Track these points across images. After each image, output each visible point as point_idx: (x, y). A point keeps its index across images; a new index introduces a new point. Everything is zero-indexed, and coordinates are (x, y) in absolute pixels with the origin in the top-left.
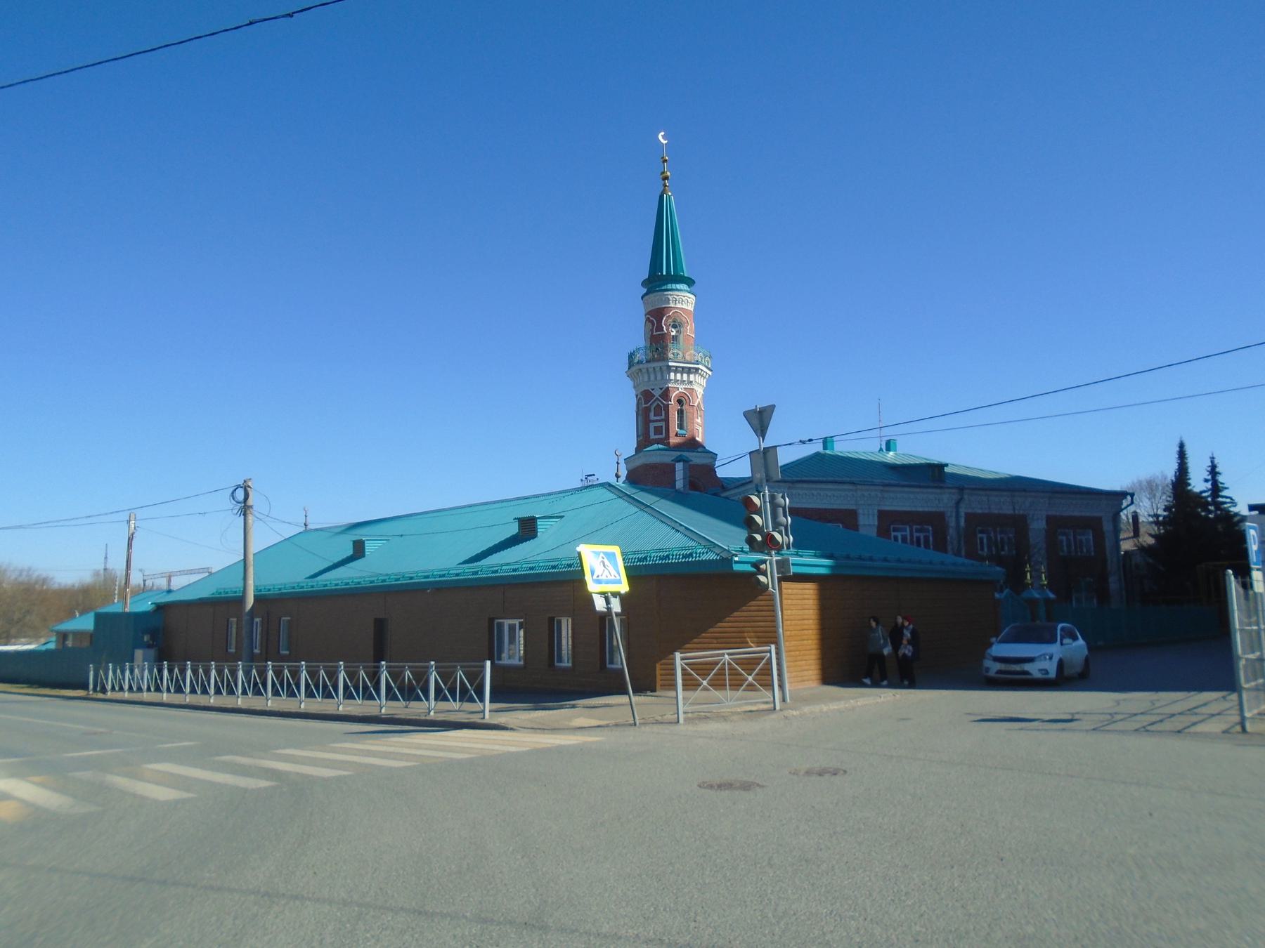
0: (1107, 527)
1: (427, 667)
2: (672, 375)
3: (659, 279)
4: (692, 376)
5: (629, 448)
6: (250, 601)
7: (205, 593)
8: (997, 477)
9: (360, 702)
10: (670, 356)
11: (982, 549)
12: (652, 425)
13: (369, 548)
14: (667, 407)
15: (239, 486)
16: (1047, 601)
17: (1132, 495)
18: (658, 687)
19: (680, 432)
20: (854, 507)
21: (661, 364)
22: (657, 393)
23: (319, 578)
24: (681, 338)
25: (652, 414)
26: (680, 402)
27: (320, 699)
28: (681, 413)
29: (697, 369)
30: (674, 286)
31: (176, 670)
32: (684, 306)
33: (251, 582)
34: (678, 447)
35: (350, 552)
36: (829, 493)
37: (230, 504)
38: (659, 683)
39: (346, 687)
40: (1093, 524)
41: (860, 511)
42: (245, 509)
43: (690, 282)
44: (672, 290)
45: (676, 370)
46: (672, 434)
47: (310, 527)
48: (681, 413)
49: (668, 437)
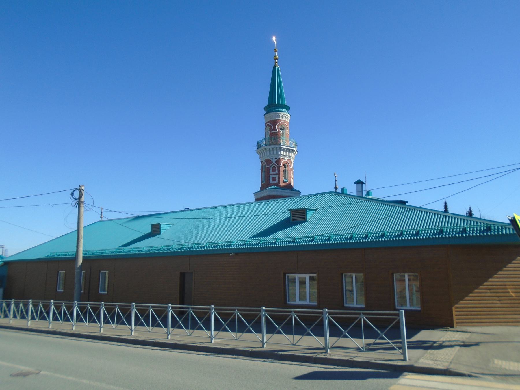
1: (10, 302)
2: (282, 152)
3: (274, 105)
4: (290, 154)
5: (258, 188)
6: (80, 261)
7: (42, 254)
9: (87, 324)
10: (281, 143)
12: (271, 177)
13: (163, 228)
14: (279, 168)
15: (76, 189)
18: (455, 324)
19: (285, 180)
21: (277, 146)
22: (274, 161)
23: (131, 246)
25: (271, 171)
26: (284, 166)
27: (61, 322)
28: (285, 171)
29: (293, 150)
30: (282, 110)
31: (21, 305)
32: (286, 120)
33: (81, 248)
34: (284, 188)
35: (149, 230)
37: (70, 200)
38: (455, 321)
39: (78, 315)
42: (79, 203)
43: (288, 108)
44: (281, 111)
45: (284, 150)
46: (281, 181)
47: (103, 219)
48: (285, 171)
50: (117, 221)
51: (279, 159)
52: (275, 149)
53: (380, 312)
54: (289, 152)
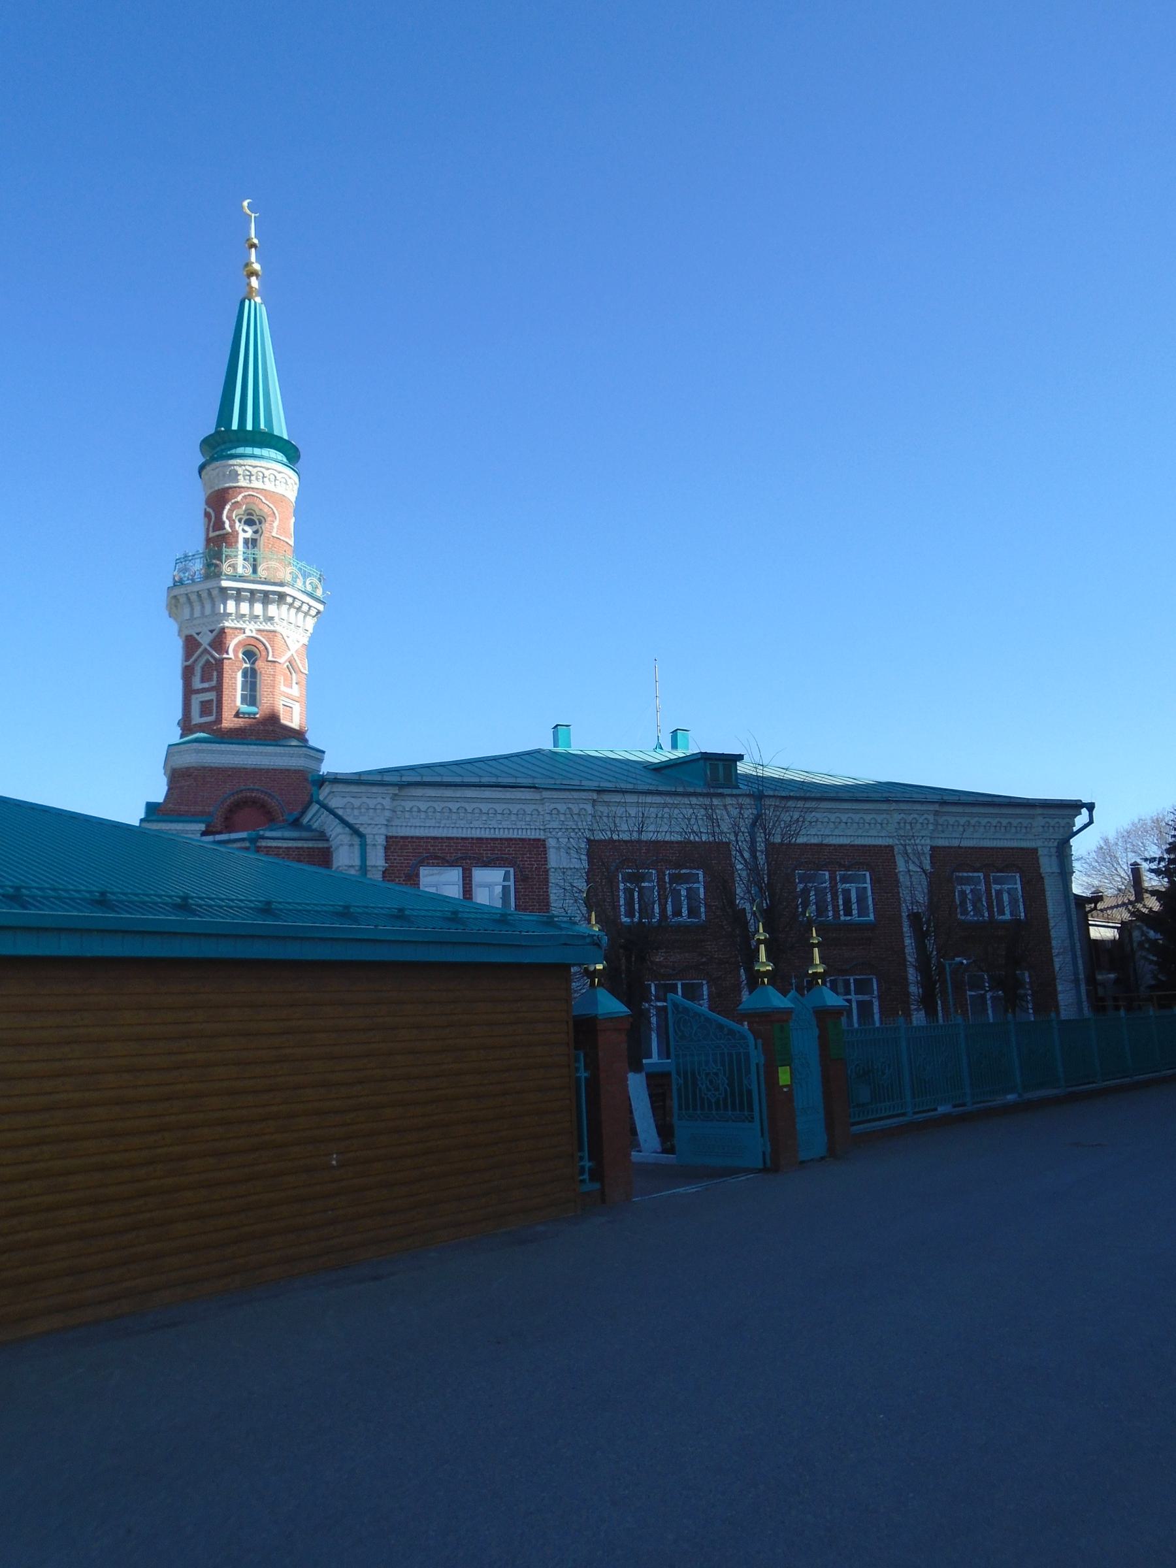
0: (1047, 865)
8: (850, 782)
11: (1002, 913)
16: (824, 1015)
17: (1091, 807)
20: (541, 835)
21: (210, 584)
22: (205, 640)
24: (262, 542)
26: (250, 655)
28: (251, 676)
30: (249, 450)
32: (269, 486)
36: (485, 807)
40: (1023, 863)
41: (551, 842)
45: (238, 596)
49: (219, 720)
50: (666, 771)
51: (222, 631)
52: (204, 595)
53: (762, 1078)
54: (252, 601)
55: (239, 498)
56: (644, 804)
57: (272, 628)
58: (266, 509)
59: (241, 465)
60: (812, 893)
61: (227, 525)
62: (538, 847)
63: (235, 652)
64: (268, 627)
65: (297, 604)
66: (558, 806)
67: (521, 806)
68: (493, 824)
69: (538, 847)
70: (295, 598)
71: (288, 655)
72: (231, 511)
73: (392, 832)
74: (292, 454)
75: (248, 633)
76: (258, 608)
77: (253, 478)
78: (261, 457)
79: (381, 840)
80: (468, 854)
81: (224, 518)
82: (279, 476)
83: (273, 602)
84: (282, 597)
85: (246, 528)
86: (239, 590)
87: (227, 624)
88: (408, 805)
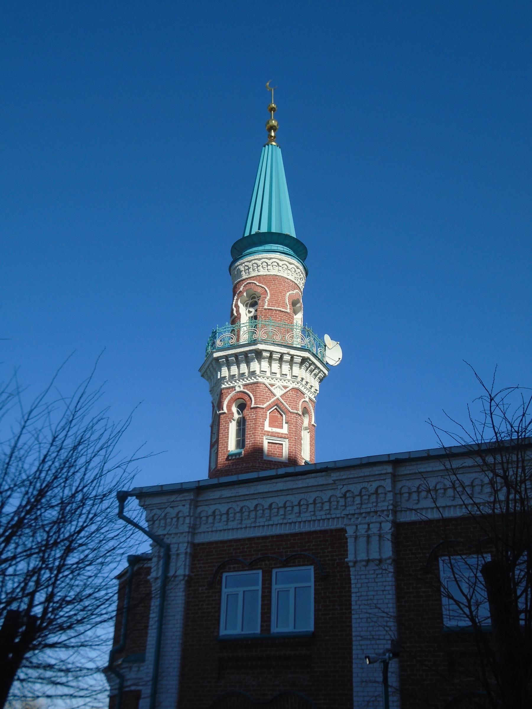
26: (242, 407)
32: (263, 272)
36: (280, 501)
41: (350, 531)
55: (241, 289)
56: (454, 471)
57: (255, 380)
58: (259, 290)
59: (241, 264)
60: (522, 616)
61: (235, 312)
62: (337, 538)
63: (229, 407)
64: (253, 380)
65: (276, 356)
66: (351, 487)
67: (302, 496)
68: (292, 518)
69: (337, 538)
70: (271, 352)
71: (275, 398)
72: (237, 299)
73: (200, 539)
74: (297, 248)
75: (238, 389)
76: (244, 368)
77: (251, 270)
78: (254, 252)
79: (183, 548)
80: (266, 555)
81: (234, 307)
82: (270, 262)
83: (252, 360)
84: (259, 354)
85: (251, 309)
86: (226, 357)
87: (223, 386)
88: (210, 510)
